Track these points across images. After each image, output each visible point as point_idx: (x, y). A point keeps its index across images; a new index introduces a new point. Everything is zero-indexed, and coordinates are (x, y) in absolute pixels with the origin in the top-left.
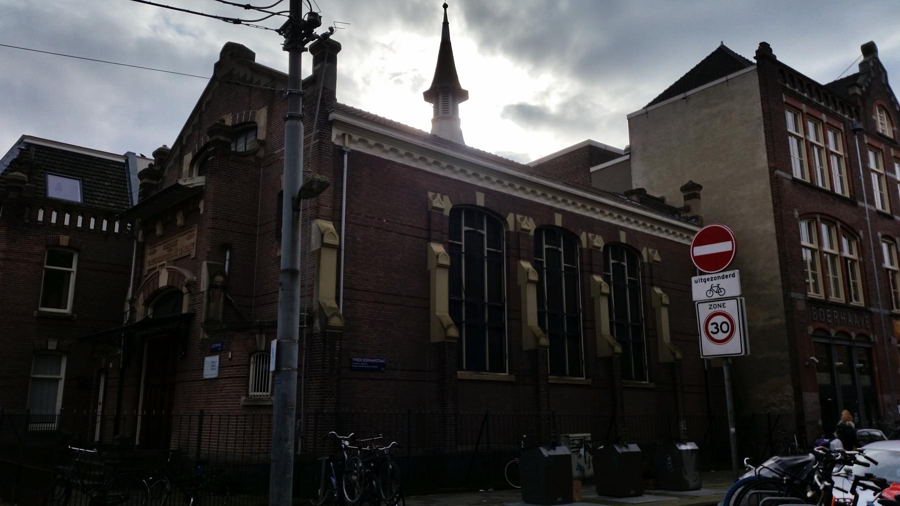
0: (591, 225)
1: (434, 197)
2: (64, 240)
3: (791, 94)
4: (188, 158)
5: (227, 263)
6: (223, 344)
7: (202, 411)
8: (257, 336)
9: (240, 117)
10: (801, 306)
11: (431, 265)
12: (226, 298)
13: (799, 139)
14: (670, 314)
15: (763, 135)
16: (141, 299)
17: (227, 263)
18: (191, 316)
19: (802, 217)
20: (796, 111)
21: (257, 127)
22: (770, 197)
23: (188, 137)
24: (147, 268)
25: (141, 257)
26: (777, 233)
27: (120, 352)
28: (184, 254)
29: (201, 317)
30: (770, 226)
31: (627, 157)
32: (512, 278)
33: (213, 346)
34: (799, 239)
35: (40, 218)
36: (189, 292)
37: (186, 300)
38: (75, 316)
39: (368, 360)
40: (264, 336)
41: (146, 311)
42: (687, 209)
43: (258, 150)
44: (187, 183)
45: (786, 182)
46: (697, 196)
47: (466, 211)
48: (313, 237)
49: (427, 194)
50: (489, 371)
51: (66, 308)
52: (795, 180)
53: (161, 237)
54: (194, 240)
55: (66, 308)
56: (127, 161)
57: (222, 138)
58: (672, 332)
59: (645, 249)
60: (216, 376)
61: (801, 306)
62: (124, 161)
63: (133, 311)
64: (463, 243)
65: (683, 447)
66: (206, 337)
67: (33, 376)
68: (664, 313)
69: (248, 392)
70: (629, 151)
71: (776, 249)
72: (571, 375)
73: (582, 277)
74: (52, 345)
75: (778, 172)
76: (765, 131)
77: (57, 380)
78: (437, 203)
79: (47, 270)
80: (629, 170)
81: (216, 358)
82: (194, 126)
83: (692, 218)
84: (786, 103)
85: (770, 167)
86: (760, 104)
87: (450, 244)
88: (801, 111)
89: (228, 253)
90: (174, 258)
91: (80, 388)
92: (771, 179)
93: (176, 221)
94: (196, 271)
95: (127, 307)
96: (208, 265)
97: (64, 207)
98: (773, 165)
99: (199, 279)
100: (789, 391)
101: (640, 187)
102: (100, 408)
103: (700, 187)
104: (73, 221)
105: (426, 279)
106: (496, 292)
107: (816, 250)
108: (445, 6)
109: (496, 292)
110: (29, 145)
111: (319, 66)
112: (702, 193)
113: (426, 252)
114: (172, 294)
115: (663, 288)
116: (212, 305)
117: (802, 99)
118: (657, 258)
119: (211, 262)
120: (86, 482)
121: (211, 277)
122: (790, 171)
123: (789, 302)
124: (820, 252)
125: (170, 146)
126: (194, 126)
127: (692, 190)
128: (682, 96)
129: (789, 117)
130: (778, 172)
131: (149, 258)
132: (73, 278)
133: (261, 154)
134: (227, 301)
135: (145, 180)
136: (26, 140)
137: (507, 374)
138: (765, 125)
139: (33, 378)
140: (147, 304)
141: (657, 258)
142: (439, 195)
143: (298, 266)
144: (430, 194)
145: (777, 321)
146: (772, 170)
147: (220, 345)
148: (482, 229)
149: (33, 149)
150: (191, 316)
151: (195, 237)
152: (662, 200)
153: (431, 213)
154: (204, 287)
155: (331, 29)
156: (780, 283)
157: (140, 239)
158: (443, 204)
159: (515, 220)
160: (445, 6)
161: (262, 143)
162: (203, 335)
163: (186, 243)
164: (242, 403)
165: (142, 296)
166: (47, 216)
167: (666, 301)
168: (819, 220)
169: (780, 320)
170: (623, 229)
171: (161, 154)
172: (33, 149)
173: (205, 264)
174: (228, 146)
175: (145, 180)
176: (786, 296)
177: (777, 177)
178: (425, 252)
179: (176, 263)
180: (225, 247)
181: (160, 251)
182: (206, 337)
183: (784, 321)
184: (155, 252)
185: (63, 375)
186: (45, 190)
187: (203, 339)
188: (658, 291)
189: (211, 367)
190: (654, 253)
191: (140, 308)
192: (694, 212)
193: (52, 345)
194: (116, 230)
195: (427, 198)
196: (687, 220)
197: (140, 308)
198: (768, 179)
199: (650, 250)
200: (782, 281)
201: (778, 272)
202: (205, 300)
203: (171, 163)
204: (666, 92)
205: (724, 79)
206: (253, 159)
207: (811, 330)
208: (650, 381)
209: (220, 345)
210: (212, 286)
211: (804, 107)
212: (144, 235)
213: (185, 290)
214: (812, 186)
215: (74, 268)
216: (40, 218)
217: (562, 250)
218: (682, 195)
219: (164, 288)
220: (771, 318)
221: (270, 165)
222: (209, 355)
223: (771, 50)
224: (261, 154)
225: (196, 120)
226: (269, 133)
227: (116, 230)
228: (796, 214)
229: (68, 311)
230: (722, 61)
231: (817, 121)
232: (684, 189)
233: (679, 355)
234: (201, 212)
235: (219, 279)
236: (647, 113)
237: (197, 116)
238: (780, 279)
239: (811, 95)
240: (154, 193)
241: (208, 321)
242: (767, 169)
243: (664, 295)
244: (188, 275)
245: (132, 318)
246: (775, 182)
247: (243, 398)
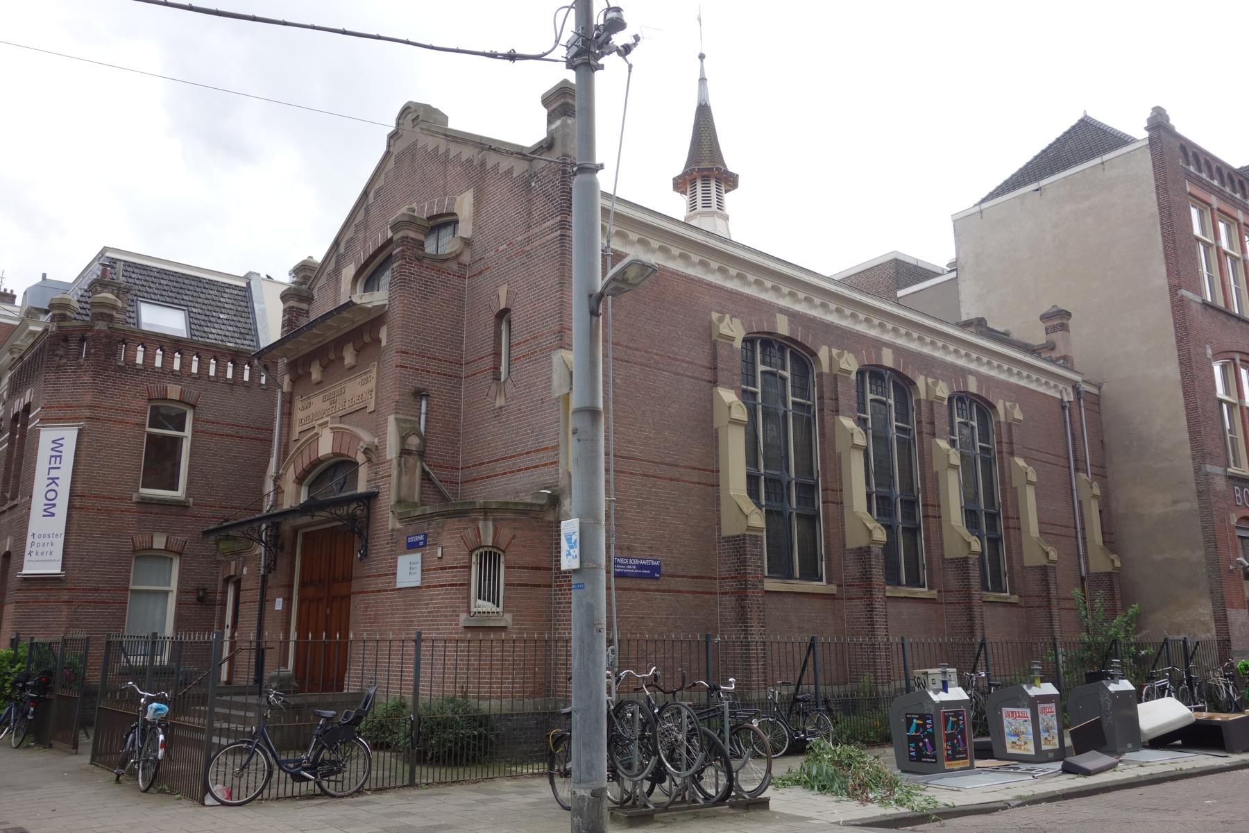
0: (928, 365)
1: (721, 320)
2: (174, 391)
3: (1198, 181)
4: (349, 271)
5: (423, 417)
6: (426, 536)
7: (419, 634)
8: (481, 524)
9: (431, 208)
10: (1220, 484)
11: (719, 420)
12: (423, 470)
13: (1207, 246)
14: (1037, 495)
15: (1160, 238)
16: (291, 475)
17: (423, 417)
18: (370, 498)
19: (1216, 356)
20: (1203, 205)
21: (457, 222)
22: (1172, 329)
23: (348, 242)
24: (297, 428)
25: (288, 414)
26: (1183, 378)
27: (261, 550)
28: (356, 407)
29: (388, 498)
30: (1171, 370)
31: (953, 275)
32: (828, 439)
33: (411, 540)
34: (1215, 389)
35: (139, 359)
36: (369, 460)
37: (363, 473)
38: (191, 500)
39: (636, 562)
40: (490, 524)
41: (298, 494)
42: (1051, 347)
43: (461, 253)
44: (363, 301)
45: (1194, 306)
46: (1064, 327)
47: (764, 342)
48: (555, 377)
49: (709, 314)
50: (800, 578)
51: (174, 487)
52: (1205, 304)
53: (352, 368)
54: (372, 384)
55: (174, 487)
56: (248, 284)
57: (412, 234)
58: (1041, 523)
59: (1001, 402)
60: (418, 584)
61: (1220, 484)
62: (244, 285)
63: (278, 490)
64: (759, 390)
65: (1112, 687)
66: (398, 526)
67: (132, 587)
68: (1030, 493)
69: (469, 607)
70: (954, 266)
71: (1182, 401)
72: (909, 584)
73: (921, 442)
74: (159, 542)
75: (1183, 292)
76: (1163, 234)
77: (166, 593)
78: (724, 329)
79: (150, 436)
80: (957, 292)
81: (416, 557)
82: (357, 226)
83: (1058, 359)
84: (1190, 194)
85: (1170, 287)
86: (1154, 196)
87: (744, 391)
88: (1209, 205)
89: (424, 403)
90: (341, 413)
91: (200, 603)
92: (1172, 302)
93: (343, 359)
94: (378, 429)
95: (269, 487)
96: (397, 419)
97: (170, 344)
98: (1175, 282)
99: (383, 441)
100: (1205, 610)
101: (973, 316)
102: (228, 633)
103: (1069, 314)
104: (185, 365)
105: (712, 440)
106: (806, 466)
107: (1235, 405)
108: (702, 57)
109: (806, 466)
110: (114, 261)
111: (558, 123)
112: (1071, 323)
113: (711, 401)
114: (341, 466)
115: (1026, 458)
116: (405, 479)
117: (1211, 189)
118: (1018, 415)
119: (400, 416)
120: (215, 740)
121: (403, 439)
122: (1199, 291)
123: (1203, 479)
124: (1241, 407)
125: (319, 258)
126: (357, 226)
127: (1058, 319)
128: (1034, 186)
129: (1194, 213)
130: (1183, 292)
131: (299, 415)
132: (186, 447)
133: (466, 258)
134: (425, 476)
135: (292, 303)
136: (108, 254)
137: (824, 582)
138: (1162, 224)
139: (134, 591)
140: (300, 480)
141: (1018, 415)
142: (727, 316)
143: (601, 406)
144: (715, 316)
145: (1186, 506)
146: (1174, 290)
147: (422, 538)
148: (784, 368)
149: (120, 267)
150: (370, 498)
151: (374, 381)
152: (1006, 334)
153: (713, 343)
154: (391, 450)
155: (637, 38)
156: (1189, 452)
157: (286, 386)
158: (733, 329)
159: (831, 357)
160: (702, 57)
161: (467, 242)
162: (393, 523)
163: (358, 389)
164: (462, 624)
165: (292, 469)
166: (149, 357)
167: (1033, 477)
168: (1238, 362)
169: (1190, 504)
170: (971, 372)
171: (304, 271)
172: (120, 267)
173: (391, 419)
174: (421, 245)
175: (292, 303)
176: (1197, 470)
177: (1182, 299)
178: (708, 405)
179: (354, 420)
180: (419, 394)
181: (318, 403)
182: (398, 526)
183: (1196, 505)
184: (309, 406)
185: (174, 586)
186: (138, 323)
187: (393, 530)
188: (1021, 462)
189: (408, 571)
190: (1013, 407)
191: (289, 485)
192: (1061, 350)
193: (159, 542)
194: (246, 378)
195: (711, 322)
196: (1053, 361)
197: (289, 485)
198: (1168, 301)
199: (1008, 404)
200: (1192, 449)
201: (1186, 436)
202: (395, 473)
203: (323, 281)
204: (1006, 182)
205: (1097, 161)
206: (454, 266)
207: (1234, 519)
208: (1012, 593)
209: (422, 538)
210: (404, 452)
211: (1213, 200)
212: (294, 382)
213: (360, 458)
214: (1226, 313)
215: (188, 431)
216: (139, 359)
217: (891, 402)
218: (1042, 326)
219: (327, 458)
220: (1175, 502)
221: (480, 273)
222: (405, 553)
223: (1167, 118)
224: (466, 258)
225: (360, 217)
226: (477, 227)
227: (246, 378)
228: (1209, 352)
229: (179, 494)
230: (1087, 140)
231: (1230, 219)
232: (1044, 318)
233: (1053, 555)
234: (384, 343)
235: (414, 442)
236: (981, 212)
237: (362, 212)
238: (1188, 446)
239: (1222, 182)
240: (303, 322)
241: (399, 502)
242: (1167, 287)
243: (1030, 469)
244: (367, 438)
245: (276, 504)
246: (1179, 306)
247: (463, 616)
